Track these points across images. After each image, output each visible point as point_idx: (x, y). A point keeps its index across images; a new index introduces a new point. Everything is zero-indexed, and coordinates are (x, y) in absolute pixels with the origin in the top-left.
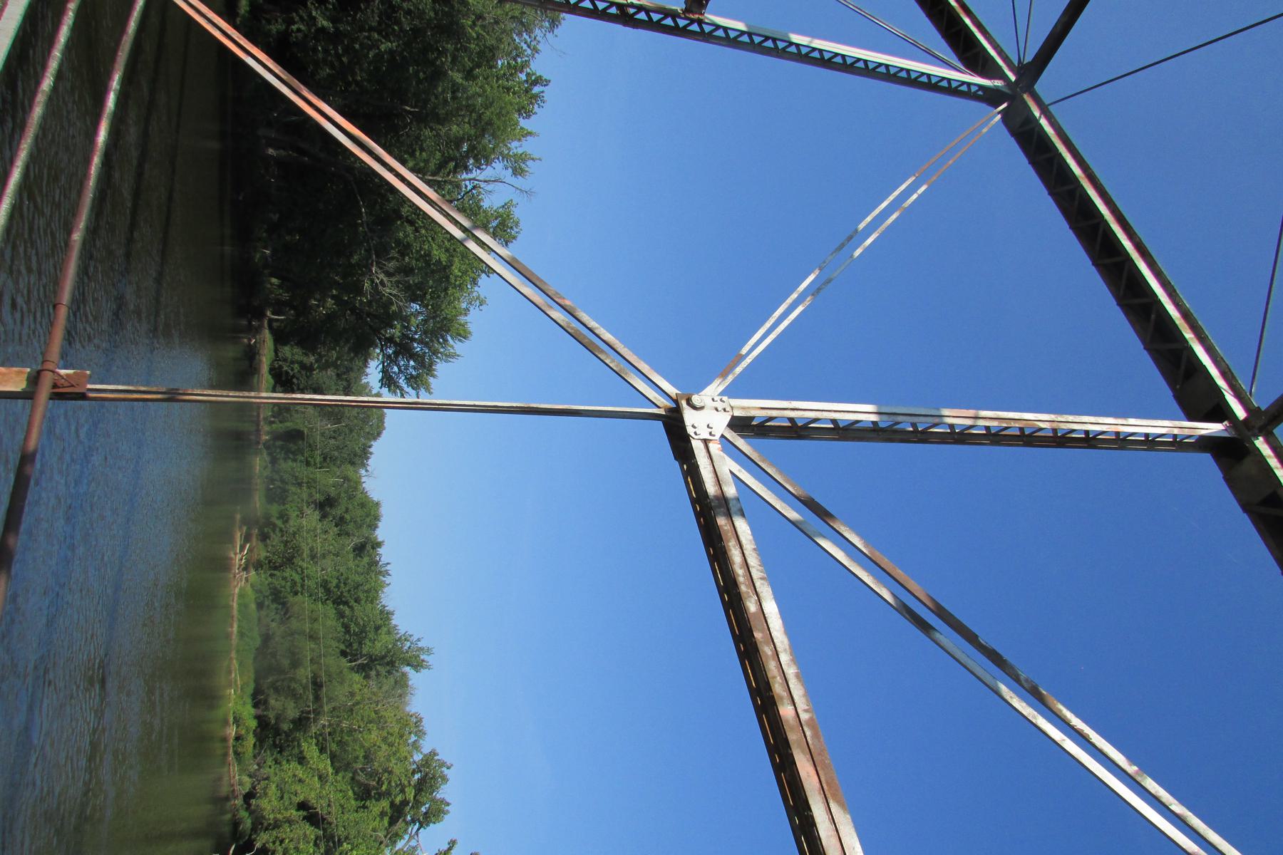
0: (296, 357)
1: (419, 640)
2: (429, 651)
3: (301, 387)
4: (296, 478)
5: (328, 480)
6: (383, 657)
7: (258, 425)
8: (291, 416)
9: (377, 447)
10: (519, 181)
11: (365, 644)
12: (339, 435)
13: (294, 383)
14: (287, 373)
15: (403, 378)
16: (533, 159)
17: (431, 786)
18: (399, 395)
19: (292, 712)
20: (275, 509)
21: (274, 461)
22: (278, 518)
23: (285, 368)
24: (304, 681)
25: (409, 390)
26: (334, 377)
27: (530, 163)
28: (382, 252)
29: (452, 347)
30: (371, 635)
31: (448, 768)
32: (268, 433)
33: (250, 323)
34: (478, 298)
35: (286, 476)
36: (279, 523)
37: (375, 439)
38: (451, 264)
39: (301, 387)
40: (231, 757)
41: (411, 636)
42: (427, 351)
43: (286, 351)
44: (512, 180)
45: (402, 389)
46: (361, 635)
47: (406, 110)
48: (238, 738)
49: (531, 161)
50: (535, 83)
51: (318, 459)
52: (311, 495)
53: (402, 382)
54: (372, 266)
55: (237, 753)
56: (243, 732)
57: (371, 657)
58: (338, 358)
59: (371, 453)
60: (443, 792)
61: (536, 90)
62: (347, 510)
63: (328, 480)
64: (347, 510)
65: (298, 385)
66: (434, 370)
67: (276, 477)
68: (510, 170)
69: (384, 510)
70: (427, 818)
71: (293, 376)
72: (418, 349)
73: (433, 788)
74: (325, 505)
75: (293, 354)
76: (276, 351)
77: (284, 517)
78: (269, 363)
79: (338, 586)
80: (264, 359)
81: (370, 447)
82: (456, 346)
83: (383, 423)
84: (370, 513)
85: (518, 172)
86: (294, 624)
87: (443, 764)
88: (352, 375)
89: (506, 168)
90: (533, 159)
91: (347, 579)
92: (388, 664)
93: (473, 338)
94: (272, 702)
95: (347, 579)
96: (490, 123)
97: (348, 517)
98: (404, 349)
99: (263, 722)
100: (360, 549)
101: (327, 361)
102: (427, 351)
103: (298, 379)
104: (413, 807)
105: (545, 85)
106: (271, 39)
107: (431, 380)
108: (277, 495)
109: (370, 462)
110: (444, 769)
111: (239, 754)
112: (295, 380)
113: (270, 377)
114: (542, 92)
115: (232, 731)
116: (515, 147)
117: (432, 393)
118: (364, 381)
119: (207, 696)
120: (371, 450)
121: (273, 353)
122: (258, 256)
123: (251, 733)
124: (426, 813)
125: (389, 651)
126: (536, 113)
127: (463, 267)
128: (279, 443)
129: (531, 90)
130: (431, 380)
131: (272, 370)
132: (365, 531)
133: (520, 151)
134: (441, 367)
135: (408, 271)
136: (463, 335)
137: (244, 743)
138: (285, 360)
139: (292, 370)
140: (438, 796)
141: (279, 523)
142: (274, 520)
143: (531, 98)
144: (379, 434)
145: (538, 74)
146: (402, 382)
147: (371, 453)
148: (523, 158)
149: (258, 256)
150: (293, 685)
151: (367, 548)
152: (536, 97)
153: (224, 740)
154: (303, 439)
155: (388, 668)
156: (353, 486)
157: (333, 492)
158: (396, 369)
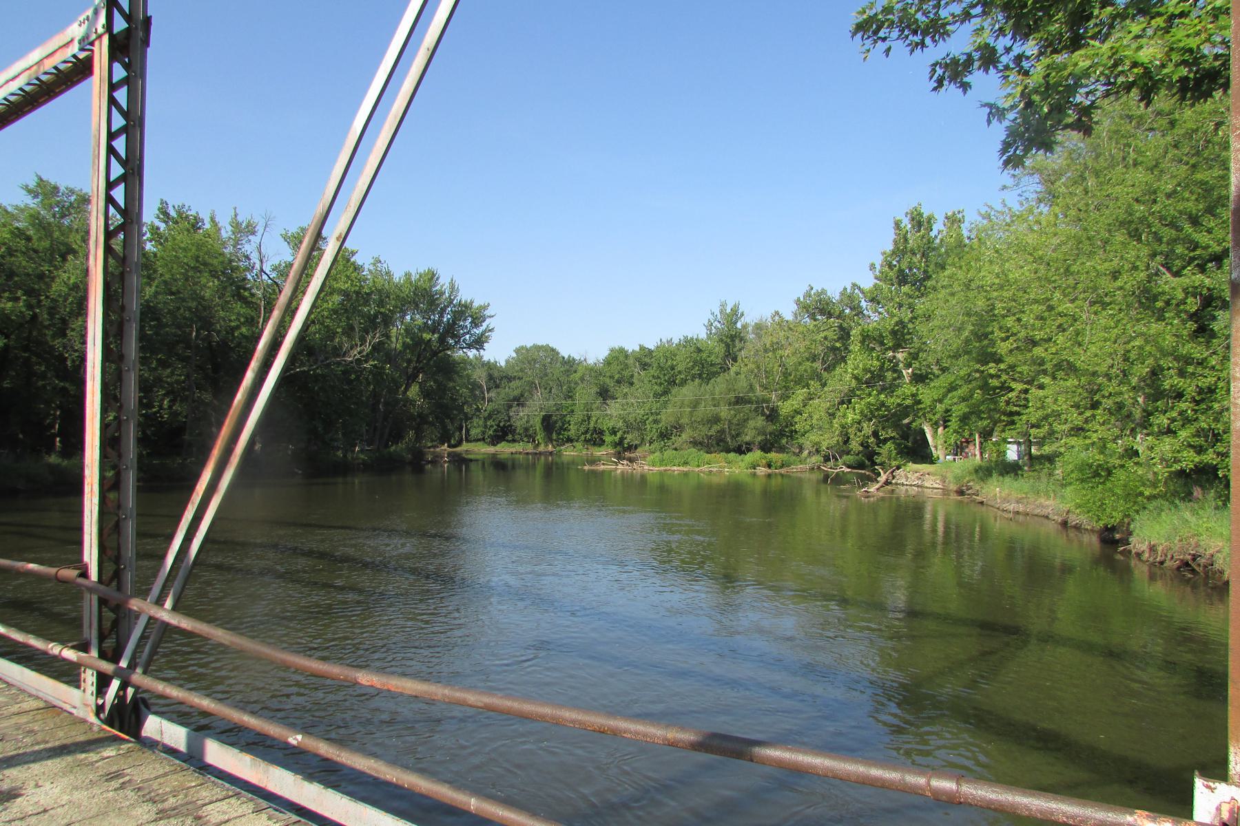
0: (481, 423)
1: (713, 314)
2: (723, 305)
3: (506, 418)
4: (583, 421)
5: (585, 395)
6: (728, 346)
7: (540, 453)
8: (531, 426)
9: (565, 353)
10: (260, 229)
11: (712, 361)
12: (549, 384)
13: (504, 425)
14: (495, 431)
15: (475, 330)
16: (236, 216)
17: (827, 304)
18: (490, 333)
19: (760, 421)
20: (608, 438)
21: (570, 440)
22: (616, 436)
23: (491, 432)
24: (732, 412)
25: (485, 325)
26: (498, 390)
27: (240, 219)
28: (337, 351)
29: (442, 287)
30: (704, 355)
31: (812, 289)
32: (546, 445)
33: (429, 462)
34: (374, 265)
35: (582, 429)
36: (619, 435)
37: (558, 353)
38: (340, 292)
39: (506, 418)
40: (783, 471)
41: (709, 321)
42: (449, 309)
43: (474, 432)
44: (259, 234)
45: (485, 332)
46: (702, 364)
47: (196, 336)
48: (769, 466)
49: (238, 217)
50: (166, 214)
51: (570, 402)
52: (598, 408)
53: (478, 331)
54: (345, 361)
55: (782, 466)
56: (764, 461)
57: (727, 356)
58: (467, 388)
59: (569, 356)
60: (834, 293)
61: (173, 213)
62: (612, 377)
63: (585, 395)
64: (612, 377)
65: (505, 421)
66: (466, 302)
67: (583, 437)
68: (250, 237)
69: (616, 346)
70: (854, 308)
71: (498, 426)
72: (449, 316)
73: (829, 302)
74: (605, 394)
75: (479, 426)
76: (478, 440)
77: (614, 432)
78: (486, 446)
79: (661, 384)
80: (483, 450)
81: (564, 358)
82: (443, 283)
83: (542, 346)
84: (618, 357)
85: (251, 230)
86: (684, 421)
87: (808, 295)
88: (496, 374)
89: (250, 241)
90: (236, 216)
91: (653, 376)
92: (733, 341)
93: (434, 267)
94: (748, 438)
95: (653, 376)
96: (197, 258)
97: (616, 377)
98: (451, 330)
99: (766, 448)
100: (644, 366)
101: (470, 397)
102: (449, 309)
103: (500, 422)
104: (843, 320)
105: (167, 204)
106: (144, 452)
107: (476, 305)
108: (596, 438)
109: (577, 358)
110: (812, 293)
111: (783, 465)
112: (502, 424)
113: (499, 445)
114: (174, 207)
115: (762, 471)
116: (226, 232)
117: (489, 304)
118: (503, 364)
119: (734, 492)
120: (566, 357)
121: (479, 443)
122: (362, 456)
123: (766, 455)
124: (851, 309)
125: (721, 340)
126: (197, 213)
127: (344, 279)
128: (554, 436)
129: (173, 218)
130: (476, 305)
131: (494, 445)
132: (631, 361)
133: (230, 228)
134: (464, 296)
135: (349, 331)
136: (432, 276)
137: (774, 461)
138: (484, 433)
139: (492, 426)
140: (837, 298)
141: (619, 435)
142: (617, 439)
143: (182, 218)
144: (553, 350)
145: (158, 212)
146: (478, 331)
147: (569, 356)
148: (236, 225)
149: (362, 456)
150: (735, 421)
151: (645, 358)
152: (180, 213)
153: (769, 476)
154: (551, 416)
155: (737, 341)
156: (594, 372)
157: (595, 389)
158: (467, 337)
